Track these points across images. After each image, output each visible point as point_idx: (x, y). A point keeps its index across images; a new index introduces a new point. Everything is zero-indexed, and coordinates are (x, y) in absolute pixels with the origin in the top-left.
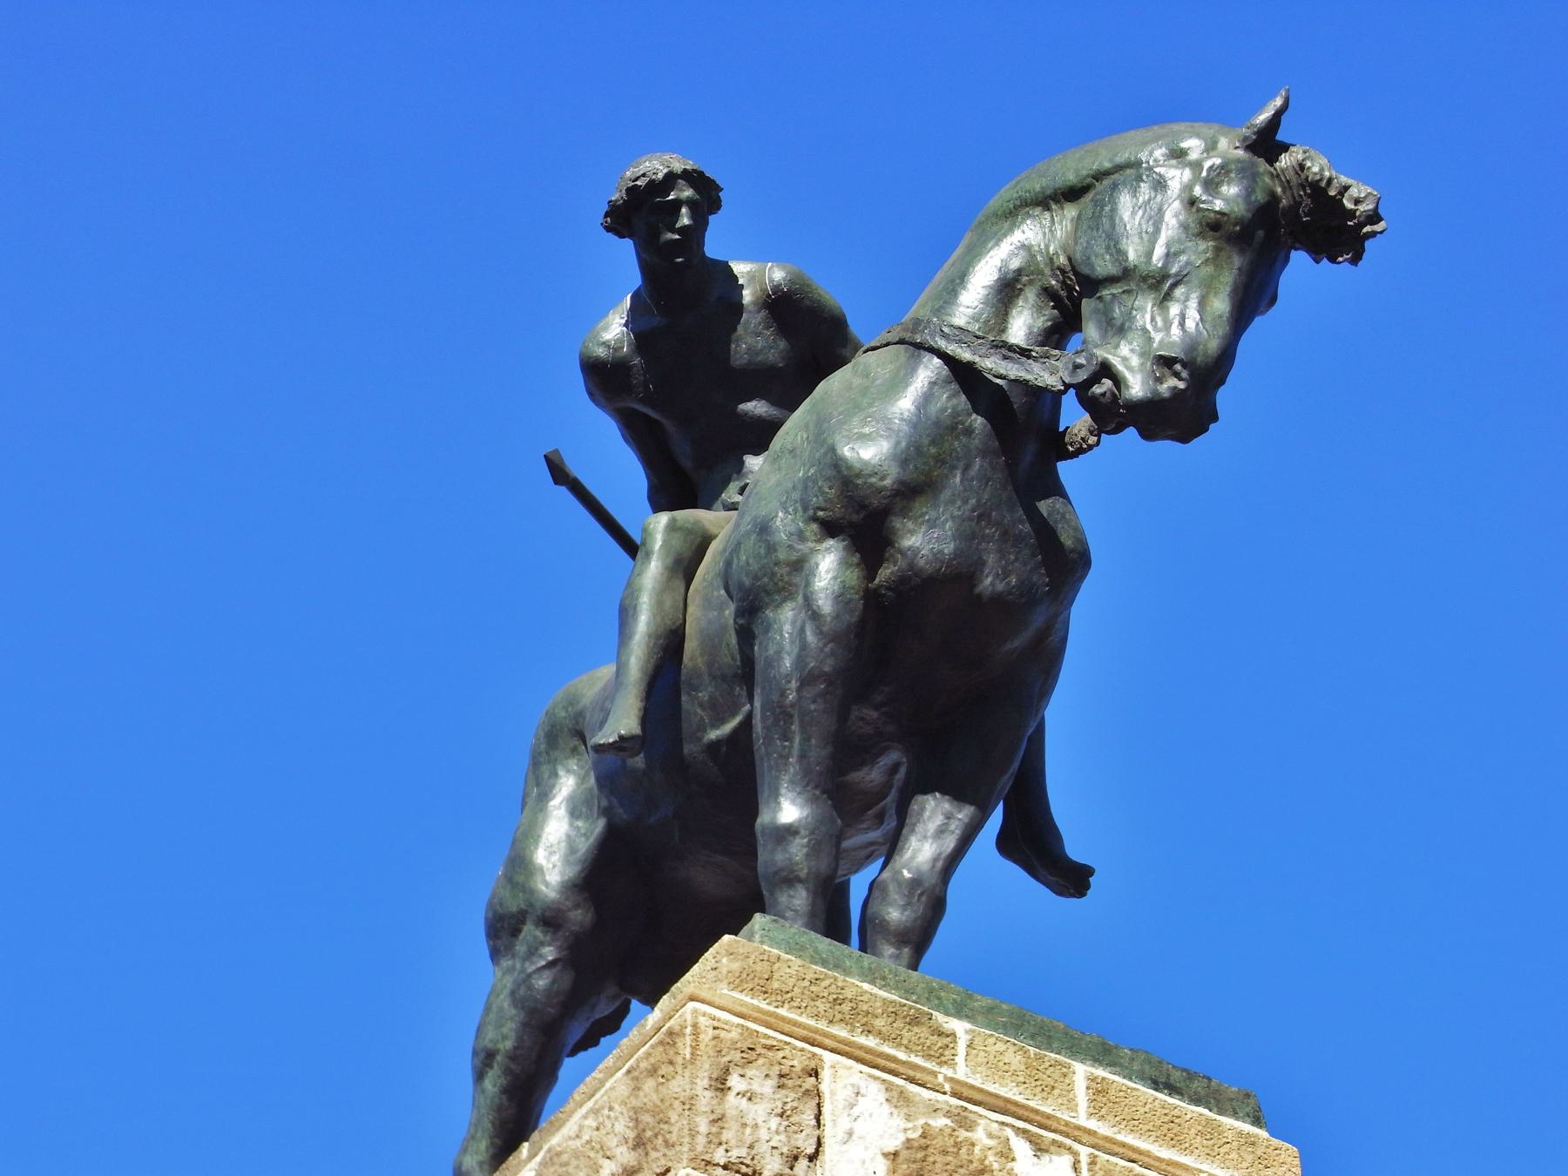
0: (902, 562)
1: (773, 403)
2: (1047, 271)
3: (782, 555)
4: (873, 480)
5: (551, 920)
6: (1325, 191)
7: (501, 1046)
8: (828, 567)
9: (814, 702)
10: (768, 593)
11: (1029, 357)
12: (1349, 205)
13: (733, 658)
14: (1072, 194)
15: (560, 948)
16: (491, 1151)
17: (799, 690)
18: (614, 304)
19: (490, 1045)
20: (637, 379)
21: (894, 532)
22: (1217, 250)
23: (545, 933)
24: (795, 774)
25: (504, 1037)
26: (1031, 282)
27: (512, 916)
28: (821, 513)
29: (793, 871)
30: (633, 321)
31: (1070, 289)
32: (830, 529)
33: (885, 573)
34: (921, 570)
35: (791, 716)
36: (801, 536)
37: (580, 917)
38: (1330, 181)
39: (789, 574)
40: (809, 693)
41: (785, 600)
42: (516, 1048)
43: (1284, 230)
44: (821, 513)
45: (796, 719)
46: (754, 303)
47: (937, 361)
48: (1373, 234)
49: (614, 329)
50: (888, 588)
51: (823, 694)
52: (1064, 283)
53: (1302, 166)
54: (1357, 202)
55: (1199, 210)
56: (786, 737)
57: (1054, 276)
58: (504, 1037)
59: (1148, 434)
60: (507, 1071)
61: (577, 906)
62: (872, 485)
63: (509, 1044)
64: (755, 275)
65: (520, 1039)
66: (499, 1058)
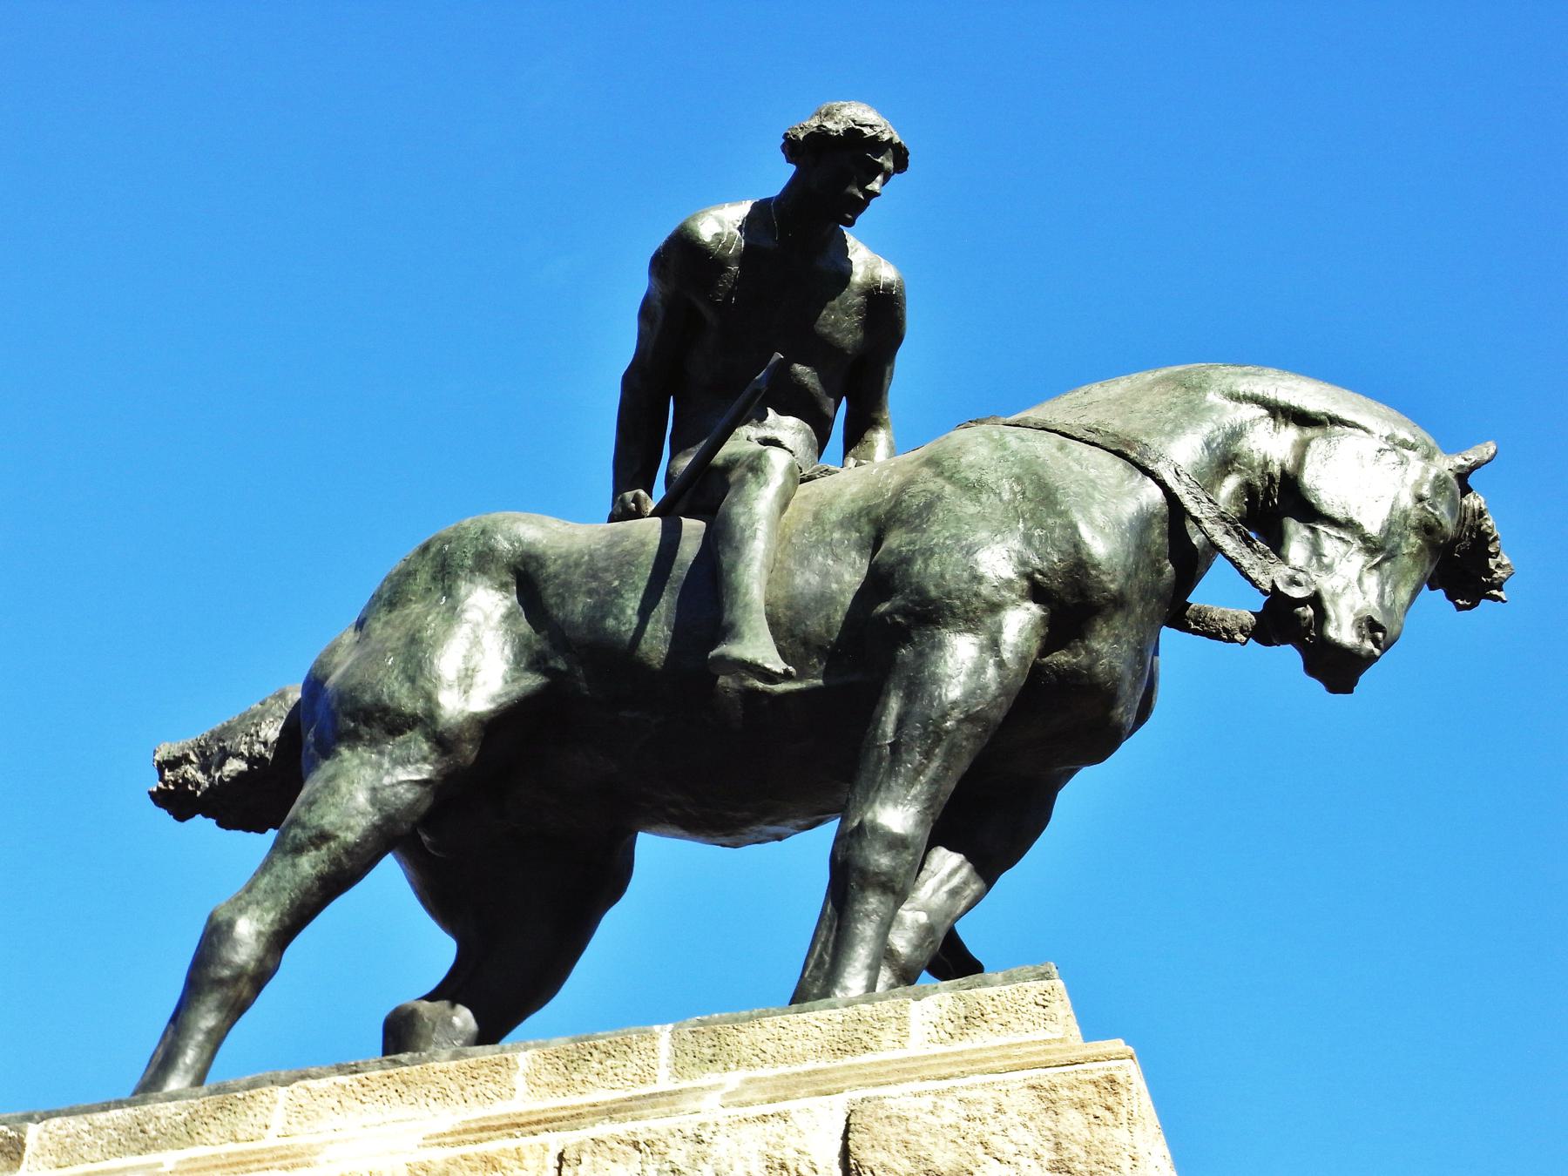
0: (1083, 658)
1: (823, 382)
2: (1258, 471)
3: (985, 590)
4: (1104, 578)
5: (443, 742)
6: (1488, 543)
7: (342, 834)
8: (1020, 623)
9: (967, 739)
10: (954, 615)
11: (1249, 546)
12: (1492, 563)
13: (828, 631)
14: (1301, 418)
15: (439, 772)
16: (276, 927)
17: (959, 722)
18: (735, 199)
19: (327, 827)
20: (726, 282)
21: (1092, 630)
22: (1421, 550)
23: (433, 750)
24: (921, 792)
25: (349, 828)
26: (1239, 471)
27: (401, 714)
28: (1038, 576)
29: (891, 880)
30: (748, 225)
31: (1268, 497)
32: (1037, 592)
33: (1061, 658)
34: (1096, 675)
35: (941, 740)
36: (1009, 584)
37: (469, 751)
38: (1496, 539)
39: (984, 611)
40: (966, 728)
41: (969, 630)
42: (357, 844)
43: (1458, 562)
44: (1038, 576)
45: (945, 744)
46: (859, 286)
47: (1157, 494)
48: (1496, 598)
49: (721, 223)
50: (1056, 673)
51: (977, 736)
52: (1267, 490)
53: (1481, 513)
54: (1498, 566)
55: (1424, 509)
56: (928, 755)
57: (1261, 478)
58: (349, 828)
59: (1311, 668)
60: (335, 861)
61: (472, 740)
62: (1101, 582)
63: (351, 837)
64: (867, 260)
65: (365, 839)
66: (332, 844)
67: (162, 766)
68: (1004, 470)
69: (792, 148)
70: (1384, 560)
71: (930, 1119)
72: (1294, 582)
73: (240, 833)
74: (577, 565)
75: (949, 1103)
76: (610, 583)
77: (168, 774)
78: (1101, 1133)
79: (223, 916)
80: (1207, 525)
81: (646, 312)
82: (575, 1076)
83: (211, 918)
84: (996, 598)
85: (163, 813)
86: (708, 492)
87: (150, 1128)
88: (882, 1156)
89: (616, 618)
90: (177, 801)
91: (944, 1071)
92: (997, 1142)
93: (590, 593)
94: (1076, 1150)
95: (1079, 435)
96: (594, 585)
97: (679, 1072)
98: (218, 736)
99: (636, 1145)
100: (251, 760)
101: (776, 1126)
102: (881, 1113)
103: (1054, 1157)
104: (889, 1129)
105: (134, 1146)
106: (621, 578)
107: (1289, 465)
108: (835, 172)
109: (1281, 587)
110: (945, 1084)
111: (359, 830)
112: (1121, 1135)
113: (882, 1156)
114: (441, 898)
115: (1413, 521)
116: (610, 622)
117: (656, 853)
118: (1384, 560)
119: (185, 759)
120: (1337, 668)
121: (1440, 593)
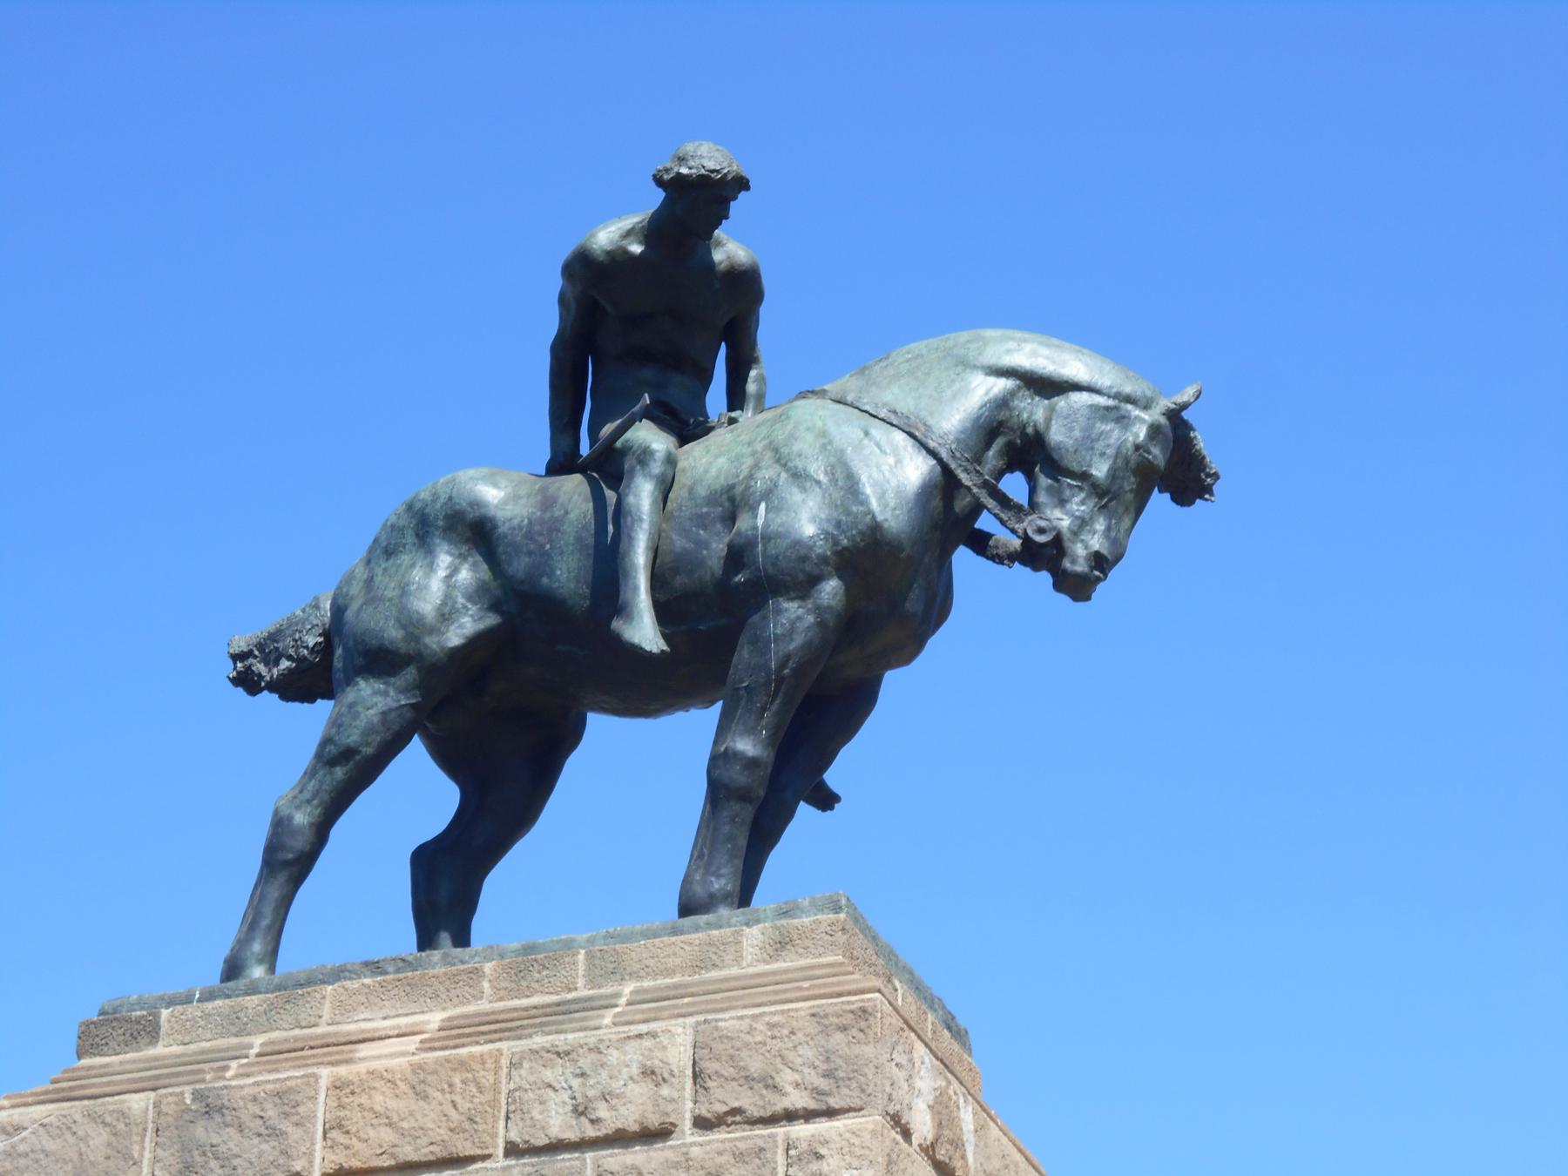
7: (364, 750)
58: (368, 744)
67: (236, 657)
68: (832, 442)
69: (659, 181)
70: (1110, 501)
71: (749, 1038)
72: (1041, 531)
73: (297, 704)
74: (520, 528)
75: (760, 1026)
76: (543, 546)
77: (239, 665)
78: (857, 1050)
79: (285, 812)
80: (975, 490)
81: (562, 301)
82: (524, 983)
83: (276, 812)
84: (816, 572)
85: (240, 690)
86: (609, 468)
87: (241, 1015)
88: (716, 1066)
89: (549, 577)
90: (248, 682)
91: (759, 1000)
92: (791, 1055)
93: (530, 553)
94: (840, 1062)
95: (882, 415)
96: (532, 547)
97: (592, 982)
98: (274, 637)
99: (558, 1054)
100: (300, 660)
101: (647, 1043)
102: (716, 1034)
103: (825, 1067)
104: (721, 1047)
105: (234, 1029)
106: (550, 541)
107: (1041, 427)
108: (695, 203)
109: (1029, 532)
110: (757, 1011)
111: (375, 744)
112: (868, 1050)
113: (716, 1066)
114: (448, 759)
115: (1133, 464)
116: (545, 580)
117: (597, 723)
118: (1110, 501)
119: (249, 654)
120: (1076, 587)
121: (1167, 495)
